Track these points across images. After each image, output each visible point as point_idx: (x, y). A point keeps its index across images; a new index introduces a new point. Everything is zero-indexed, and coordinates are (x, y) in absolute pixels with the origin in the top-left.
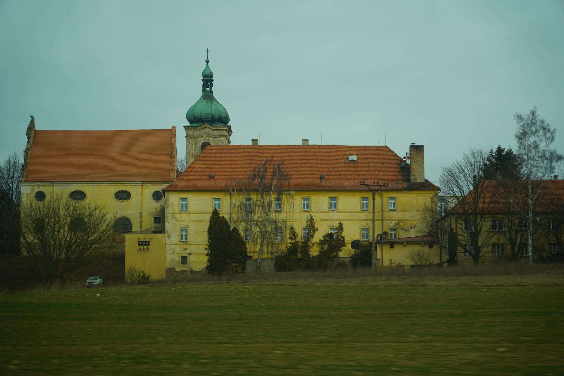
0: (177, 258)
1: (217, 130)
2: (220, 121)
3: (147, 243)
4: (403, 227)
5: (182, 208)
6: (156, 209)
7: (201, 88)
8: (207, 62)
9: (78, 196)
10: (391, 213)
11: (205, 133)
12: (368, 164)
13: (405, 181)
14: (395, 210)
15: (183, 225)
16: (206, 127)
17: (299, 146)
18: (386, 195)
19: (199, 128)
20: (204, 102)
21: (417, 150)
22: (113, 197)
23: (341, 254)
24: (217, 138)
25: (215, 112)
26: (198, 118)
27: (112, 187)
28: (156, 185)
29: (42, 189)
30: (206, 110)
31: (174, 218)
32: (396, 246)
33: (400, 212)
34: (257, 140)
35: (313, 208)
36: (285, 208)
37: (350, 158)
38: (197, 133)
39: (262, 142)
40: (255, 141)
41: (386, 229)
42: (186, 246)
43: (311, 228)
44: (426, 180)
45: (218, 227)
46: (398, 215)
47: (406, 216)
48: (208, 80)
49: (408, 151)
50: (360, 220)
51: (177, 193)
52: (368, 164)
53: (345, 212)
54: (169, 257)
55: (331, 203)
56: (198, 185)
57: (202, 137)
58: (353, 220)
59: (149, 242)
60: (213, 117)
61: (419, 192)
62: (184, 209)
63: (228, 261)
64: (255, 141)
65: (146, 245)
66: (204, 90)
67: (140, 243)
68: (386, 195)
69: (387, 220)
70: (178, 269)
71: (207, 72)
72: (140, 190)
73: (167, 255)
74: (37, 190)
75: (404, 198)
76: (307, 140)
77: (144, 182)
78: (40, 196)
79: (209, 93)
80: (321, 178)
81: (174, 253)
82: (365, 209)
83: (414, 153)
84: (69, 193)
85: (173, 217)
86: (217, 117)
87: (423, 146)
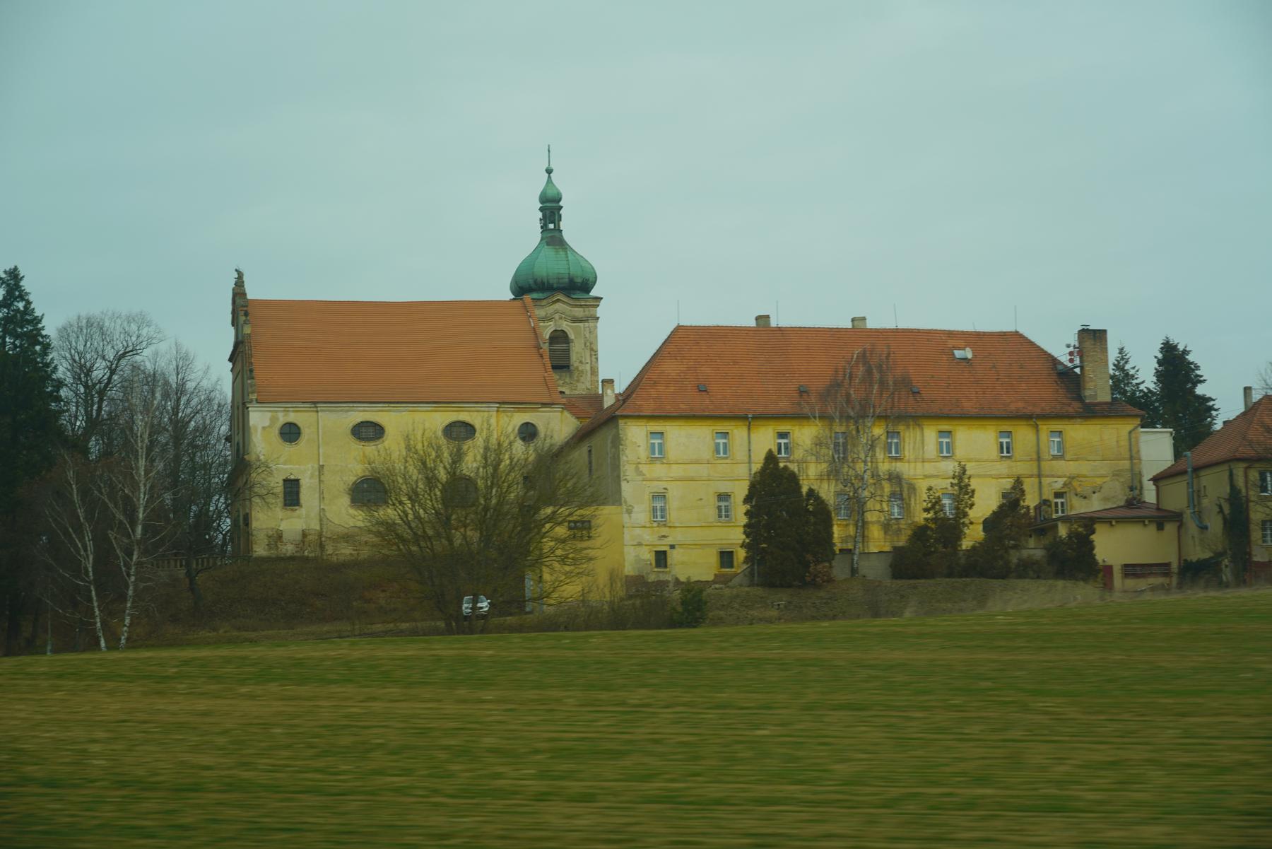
0: (648, 556)
2: (577, 288)
3: (586, 525)
4: (1079, 490)
8: (549, 171)
12: (994, 367)
14: (1061, 457)
15: (658, 487)
17: (846, 330)
18: (1045, 427)
19: (544, 303)
20: (549, 251)
22: (281, 441)
23: (966, 544)
24: (581, 321)
25: (576, 272)
26: (543, 283)
29: (292, 417)
30: (551, 265)
31: (640, 473)
34: (768, 317)
35: (960, 452)
36: (908, 452)
37: (958, 354)
39: (780, 320)
40: (763, 319)
41: (1048, 495)
42: (664, 531)
43: (963, 489)
45: (773, 490)
47: (1083, 468)
48: (551, 209)
49: (1074, 341)
50: (998, 477)
51: (643, 422)
52: (994, 367)
55: (1001, 444)
56: (682, 406)
57: (550, 320)
58: (985, 476)
60: (571, 280)
62: (658, 454)
63: (810, 557)
64: (763, 319)
66: (544, 228)
68: (1045, 427)
71: (550, 193)
73: (626, 549)
74: (282, 419)
75: (1080, 433)
76: (864, 319)
77: (504, 403)
79: (556, 234)
81: (640, 544)
83: (1088, 344)
84: (351, 426)
86: (579, 280)
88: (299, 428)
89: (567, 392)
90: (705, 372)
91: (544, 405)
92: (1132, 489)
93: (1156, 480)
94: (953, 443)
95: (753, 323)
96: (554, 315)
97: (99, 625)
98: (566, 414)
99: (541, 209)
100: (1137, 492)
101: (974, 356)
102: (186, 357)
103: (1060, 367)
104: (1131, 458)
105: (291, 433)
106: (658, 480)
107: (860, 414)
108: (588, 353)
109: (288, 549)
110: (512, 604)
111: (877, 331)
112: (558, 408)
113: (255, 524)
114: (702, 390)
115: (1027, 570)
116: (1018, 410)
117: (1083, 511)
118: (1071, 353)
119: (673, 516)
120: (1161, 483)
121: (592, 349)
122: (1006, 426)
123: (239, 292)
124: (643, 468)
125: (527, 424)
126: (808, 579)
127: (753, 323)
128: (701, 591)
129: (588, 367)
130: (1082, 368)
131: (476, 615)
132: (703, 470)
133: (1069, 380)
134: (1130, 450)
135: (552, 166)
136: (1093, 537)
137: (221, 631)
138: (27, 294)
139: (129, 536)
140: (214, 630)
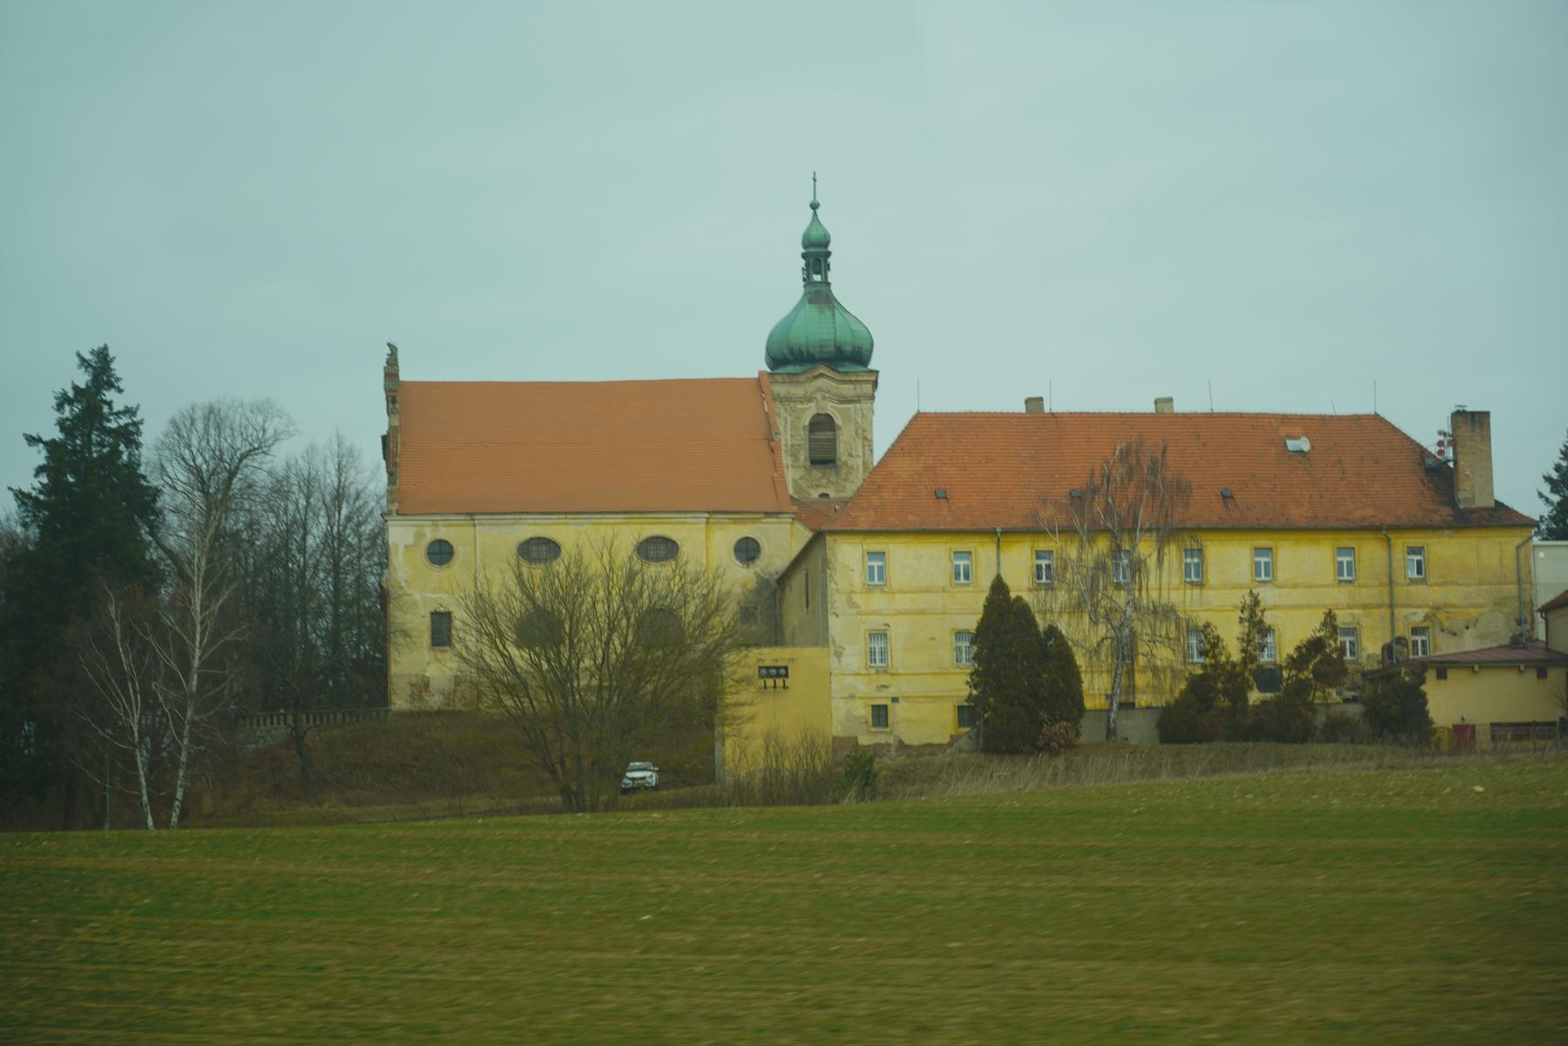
0: (864, 712)
1: (851, 382)
2: (849, 358)
4: (1446, 624)
5: (872, 578)
6: (744, 586)
7: (798, 276)
8: (814, 206)
9: (660, 549)
10: (1413, 588)
11: (819, 390)
13: (1443, 503)
14: (1424, 581)
15: (875, 622)
16: (821, 375)
17: (1150, 415)
18: (1401, 542)
19: (802, 378)
20: (811, 311)
21: (1471, 424)
22: (427, 563)
24: (850, 402)
25: (844, 337)
26: (801, 353)
27: (626, 528)
28: (743, 521)
29: (443, 533)
30: (816, 330)
31: (851, 603)
32: (1452, 674)
33: (1437, 584)
37: (1292, 445)
38: (798, 391)
40: (1034, 403)
41: (1403, 630)
42: (884, 679)
44: (1497, 502)
46: (1431, 594)
47: (1454, 595)
48: (817, 255)
49: (1447, 428)
51: (858, 539)
52: (1340, 462)
53: (1295, 586)
54: (840, 708)
56: (911, 518)
57: (810, 400)
59: (786, 668)
60: (838, 349)
61: (1484, 533)
62: (878, 578)
64: (1034, 403)
65: (778, 675)
66: (808, 281)
67: (782, 671)
68: (1400, 542)
69: (1403, 606)
70: (864, 740)
71: (815, 235)
72: (702, 535)
74: (430, 535)
75: (1446, 549)
76: (1170, 400)
78: (539, 550)
79: (823, 288)
80: (1225, 497)
81: (852, 697)
82: (1346, 577)
83: (1464, 431)
85: (850, 600)
86: (848, 348)
87: (1487, 414)
88: (451, 547)
89: (832, 494)
90: (977, 471)
91: (768, 514)
92: (1519, 622)
93: (1546, 610)
94: (1274, 563)
95: (1022, 409)
96: (820, 392)
97: (145, 798)
98: (798, 526)
99: (804, 256)
100: (1527, 627)
101: (1313, 448)
102: (350, 453)
103: (1429, 461)
104: (1519, 581)
105: (441, 553)
106: (876, 613)
107: (1124, 528)
108: (860, 444)
109: (435, 701)
110: (692, 776)
111: (1184, 415)
112: (787, 519)
113: (394, 669)
114: (941, 496)
115: (1337, 730)
116: (1364, 518)
117: (1451, 651)
118: (1440, 443)
119: (897, 659)
120: (1551, 616)
121: (865, 438)
122: (1346, 541)
123: (391, 372)
124: (859, 599)
125: (747, 539)
126: (1041, 743)
127: (1022, 409)
128: (871, 761)
129: (860, 462)
130: (1455, 462)
131: (638, 788)
132: (936, 601)
133: (1439, 477)
134: (1519, 571)
135: (818, 199)
136: (1423, 687)
137: (325, 807)
138: (118, 379)
139: (178, 686)
140: (319, 804)
